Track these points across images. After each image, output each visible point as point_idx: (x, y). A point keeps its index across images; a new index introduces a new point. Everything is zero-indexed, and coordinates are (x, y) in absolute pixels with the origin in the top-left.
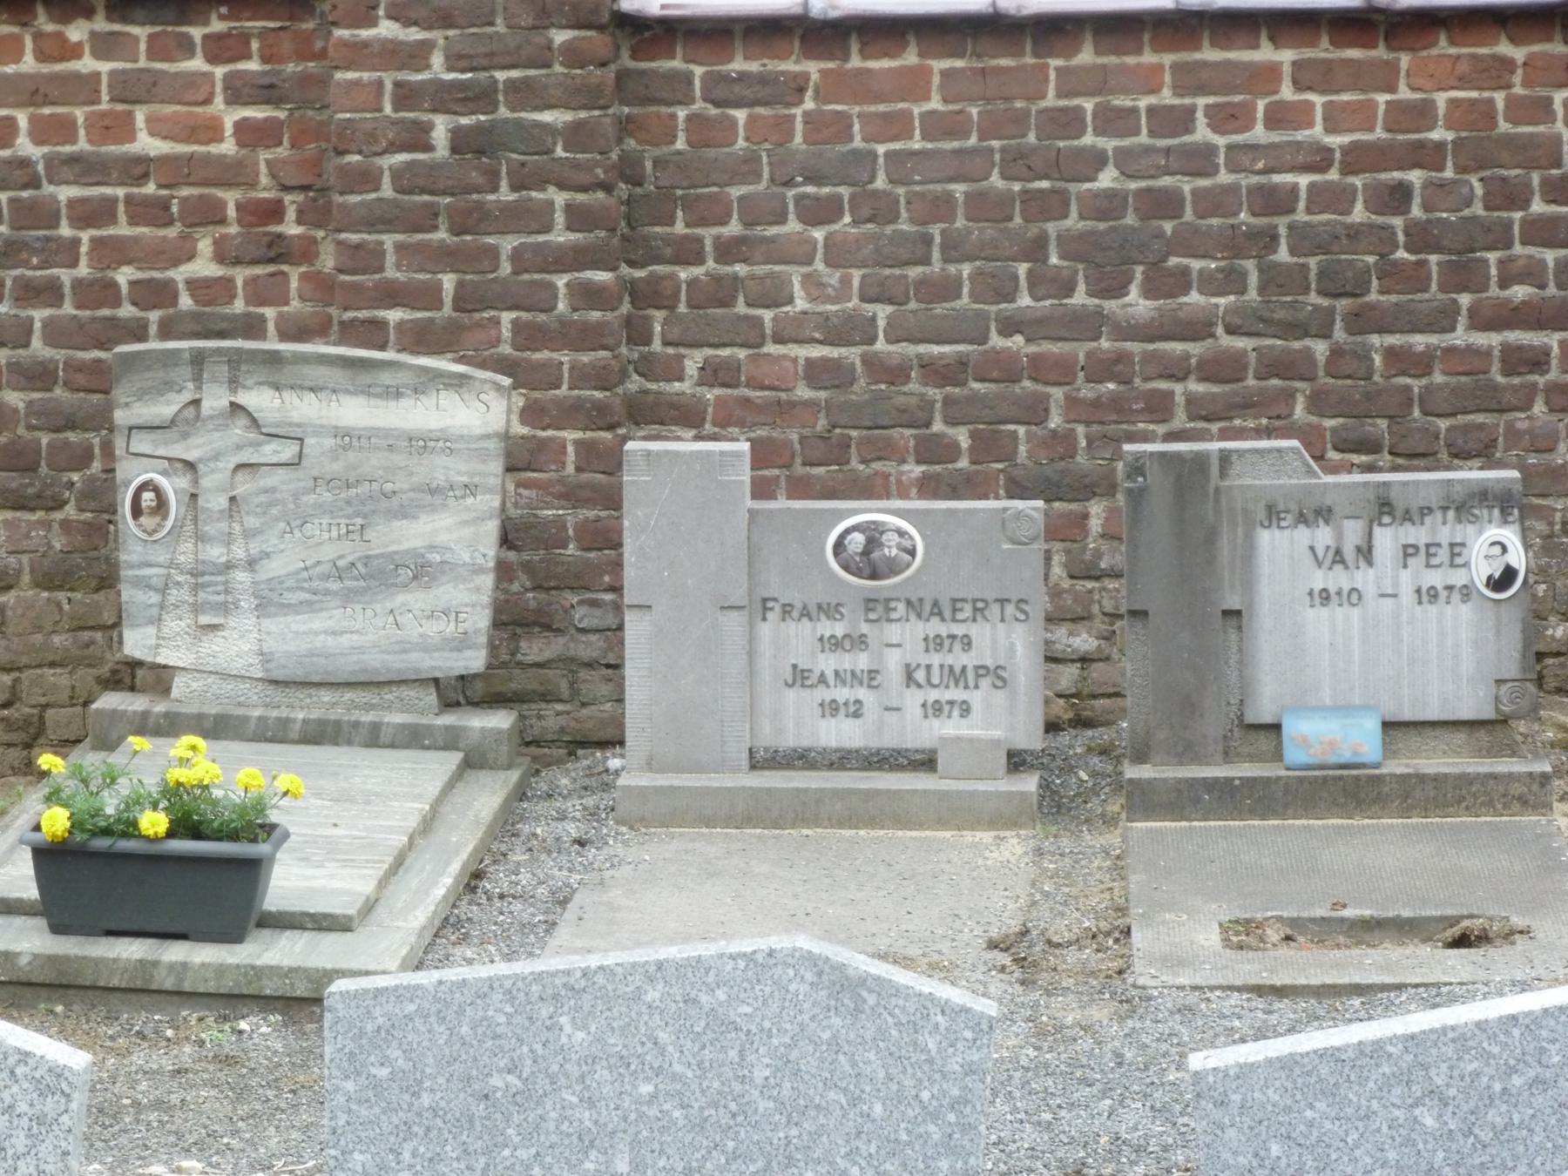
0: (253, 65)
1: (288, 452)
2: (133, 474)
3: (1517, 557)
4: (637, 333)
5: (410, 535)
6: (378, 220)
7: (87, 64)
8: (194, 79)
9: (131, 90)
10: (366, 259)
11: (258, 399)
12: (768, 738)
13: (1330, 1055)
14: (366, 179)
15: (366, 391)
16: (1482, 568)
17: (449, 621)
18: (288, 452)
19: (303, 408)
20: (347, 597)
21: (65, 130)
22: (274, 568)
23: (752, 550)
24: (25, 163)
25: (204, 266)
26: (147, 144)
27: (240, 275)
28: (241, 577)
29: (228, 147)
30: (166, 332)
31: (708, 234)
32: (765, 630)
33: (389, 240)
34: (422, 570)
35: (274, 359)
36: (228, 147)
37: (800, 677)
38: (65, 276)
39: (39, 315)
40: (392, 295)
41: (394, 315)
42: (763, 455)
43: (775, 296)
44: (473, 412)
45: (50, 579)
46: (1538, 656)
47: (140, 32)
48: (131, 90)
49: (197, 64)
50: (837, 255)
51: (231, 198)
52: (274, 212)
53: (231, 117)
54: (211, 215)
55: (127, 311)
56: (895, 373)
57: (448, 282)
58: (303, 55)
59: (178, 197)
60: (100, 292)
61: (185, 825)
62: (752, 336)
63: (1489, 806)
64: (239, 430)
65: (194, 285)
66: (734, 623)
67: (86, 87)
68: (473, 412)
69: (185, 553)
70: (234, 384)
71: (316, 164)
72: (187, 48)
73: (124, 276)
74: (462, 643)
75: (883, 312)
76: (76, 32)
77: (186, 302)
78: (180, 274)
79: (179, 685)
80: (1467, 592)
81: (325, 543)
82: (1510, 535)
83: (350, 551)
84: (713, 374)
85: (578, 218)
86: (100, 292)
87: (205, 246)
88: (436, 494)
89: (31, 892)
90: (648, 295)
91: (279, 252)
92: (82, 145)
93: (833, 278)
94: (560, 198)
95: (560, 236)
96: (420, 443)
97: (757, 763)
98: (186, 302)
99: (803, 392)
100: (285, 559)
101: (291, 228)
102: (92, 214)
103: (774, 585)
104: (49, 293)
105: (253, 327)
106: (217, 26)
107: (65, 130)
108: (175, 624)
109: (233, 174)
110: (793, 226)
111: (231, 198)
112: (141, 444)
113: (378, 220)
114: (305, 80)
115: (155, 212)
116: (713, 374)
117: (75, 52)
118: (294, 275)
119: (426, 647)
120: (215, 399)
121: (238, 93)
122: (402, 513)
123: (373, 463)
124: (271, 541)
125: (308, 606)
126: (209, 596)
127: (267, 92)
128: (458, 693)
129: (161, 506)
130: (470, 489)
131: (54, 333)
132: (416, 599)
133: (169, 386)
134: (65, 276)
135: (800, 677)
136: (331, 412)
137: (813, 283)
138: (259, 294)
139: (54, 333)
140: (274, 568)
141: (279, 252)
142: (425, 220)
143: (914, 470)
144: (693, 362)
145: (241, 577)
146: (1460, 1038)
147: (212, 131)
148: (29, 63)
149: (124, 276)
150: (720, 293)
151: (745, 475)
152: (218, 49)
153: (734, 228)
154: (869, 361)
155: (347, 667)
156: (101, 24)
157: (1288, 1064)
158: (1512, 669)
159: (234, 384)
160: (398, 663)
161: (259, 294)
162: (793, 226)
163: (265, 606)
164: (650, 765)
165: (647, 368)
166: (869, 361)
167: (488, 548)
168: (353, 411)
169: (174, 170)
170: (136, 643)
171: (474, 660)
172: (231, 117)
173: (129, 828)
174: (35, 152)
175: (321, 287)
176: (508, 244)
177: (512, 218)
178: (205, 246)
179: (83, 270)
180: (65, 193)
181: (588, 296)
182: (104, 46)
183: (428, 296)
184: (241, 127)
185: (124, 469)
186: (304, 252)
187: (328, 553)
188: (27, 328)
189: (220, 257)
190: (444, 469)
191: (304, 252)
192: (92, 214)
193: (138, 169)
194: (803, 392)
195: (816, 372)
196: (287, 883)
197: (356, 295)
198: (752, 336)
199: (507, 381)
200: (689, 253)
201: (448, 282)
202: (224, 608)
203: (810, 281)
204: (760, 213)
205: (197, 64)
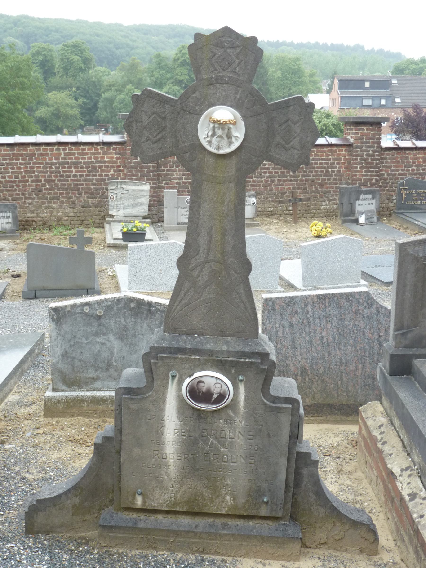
0: (118, 151)
1: (127, 192)
2: (110, 195)
3: (255, 201)
4: (158, 179)
5: (140, 201)
6: (132, 167)
7: (100, 151)
8: (111, 152)
9: (104, 154)
10: (130, 171)
11: (124, 186)
12: (179, 222)
13: (316, 244)
14: (131, 163)
15: (135, 185)
16: (252, 202)
17: (144, 210)
18: (127, 192)
19: (128, 187)
20: (133, 207)
21: (97, 158)
22: (125, 204)
23: (178, 202)
24: (93, 162)
25: (112, 172)
26: (106, 159)
27: (116, 173)
28: (122, 205)
29: (115, 160)
30: (108, 179)
31: (166, 169)
32: (179, 210)
33: (133, 169)
34: (141, 204)
35: (125, 182)
36: (115, 160)
37: (183, 215)
38: (97, 174)
39: (94, 178)
40: (133, 175)
41: (133, 177)
42: (179, 192)
43: (173, 175)
44: (146, 187)
45: (95, 206)
46: (257, 211)
47: (106, 147)
48: (104, 154)
49: (112, 151)
50: (179, 171)
51: (115, 165)
52: (120, 167)
53: (115, 156)
54: (113, 167)
55: (104, 177)
56: (185, 183)
57: (139, 174)
58: (123, 150)
59: (110, 165)
60: (101, 175)
61: (138, 230)
62: (170, 179)
63: (253, 226)
64: (121, 190)
65: (111, 175)
66: (176, 209)
67: (99, 153)
68: (146, 187)
69: (116, 203)
70: (121, 185)
71: (124, 161)
72: (111, 149)
73: (104, 174)
74: (145, 212)
75: (184, 177)
76: (99, 147)
77: (110, 176)
78: (110, 173)
79: (115, 217)
80: (250, 205)
81: (131, 202)
82: (254, 199)
83: (133, 202)
84: (166, 183)
85: (153, 167)
86: (101, 175)
87: (112, 170)
88: (142, 196)
89: (121, 237)
90: (159, 175)
91: (120, 171)
92: (99, 160)
93: (179, 173)
94: (151, 165)
95: (151, 169)
96: (141, 191)
97: (179, 224)
98: (110, 176)
99: (176, 185)
100: (325, 206)
101: (122, 168)
102: (100, 167)
103: (180, 205)
104: (96, 175)
105: (117, 179)
106: (114, 147)
107: (97, 158)
108: (115, 211)
109: (115, 162)
110: (175, 168)
111: (115, 165)
112: (111, 191)
113: (132, 167)
114: (123, 152)
115: (107, 167)
116: (166, 183)
117: (98, 149)
118: (122, 173)
119: (141, 212)
120: (119, 186)
121: (116, 154)
122: (139, 198)
123: (136, 193)
124: (125, 201)
125: (129, 208)
126: (118, 207)
127: (119, 154)
128: (145, 217)
129: (113, 198)
130: (146, 196)
131: (96, 180)
132: (140, 207)
133: (114, 185)
134: (97, 174)
135: (183, 215)
136: (131, 187)
137: (177, 174)
138: (118, 175)
139: (96, 180)
140: (125, 204)
141: (120, 171)
142: (137, 167)
143: (187, 193)
144: (164, 182)
145: (122, 205)
146: (327, 242)
147: (113, 158)
148: (93, 151)
149: (104, 174)
150: (167, 175)
151: (177, 194)
152: (114, 149)
153: (168, 168)
154: (183, 182)
155: (133, 215)
156: (101, 147)
157: (311, 245)
158: (254, 213)
159: (121, 185)
160: (138, 214)
161: (118, 175)
162: (175, 168)
163: (124, 209)
164: (167, 224)
165: (159, 183)
166: (183, 182)
167: (148, 202)
168: (134, 187)
169: (109, 162)
170: (111, 213)
171: (146, 214)
172: (115, 156)
173: (132, 230)
174: (94, 160)
175: (125, 175)
176: (146, 170)
177: (147, 167)
178: (112, 170)
179: (99, 173)
180: (97, 165)
181: (154, 175)
182: (102, 149)
183: (137, 175)
184: (116, 157)
185: (109, 194)
186: (123, 171)
187: (131, 203)
188: (93, 179)
189: (114, 171)
190: (143, 193)
191: (123, 171)
192: (100, 167)
193: (105, 162)
194: (176, 185)
195: (177, 183)
196: (147, 236)
197: (129, 175)
198: (170, 179)
199: (370, 196)
200: (164, 170)
201: (139, 174)
202: (120, 209)
203: (176, 174)
204: (171, 166)
205: (112, 151)
